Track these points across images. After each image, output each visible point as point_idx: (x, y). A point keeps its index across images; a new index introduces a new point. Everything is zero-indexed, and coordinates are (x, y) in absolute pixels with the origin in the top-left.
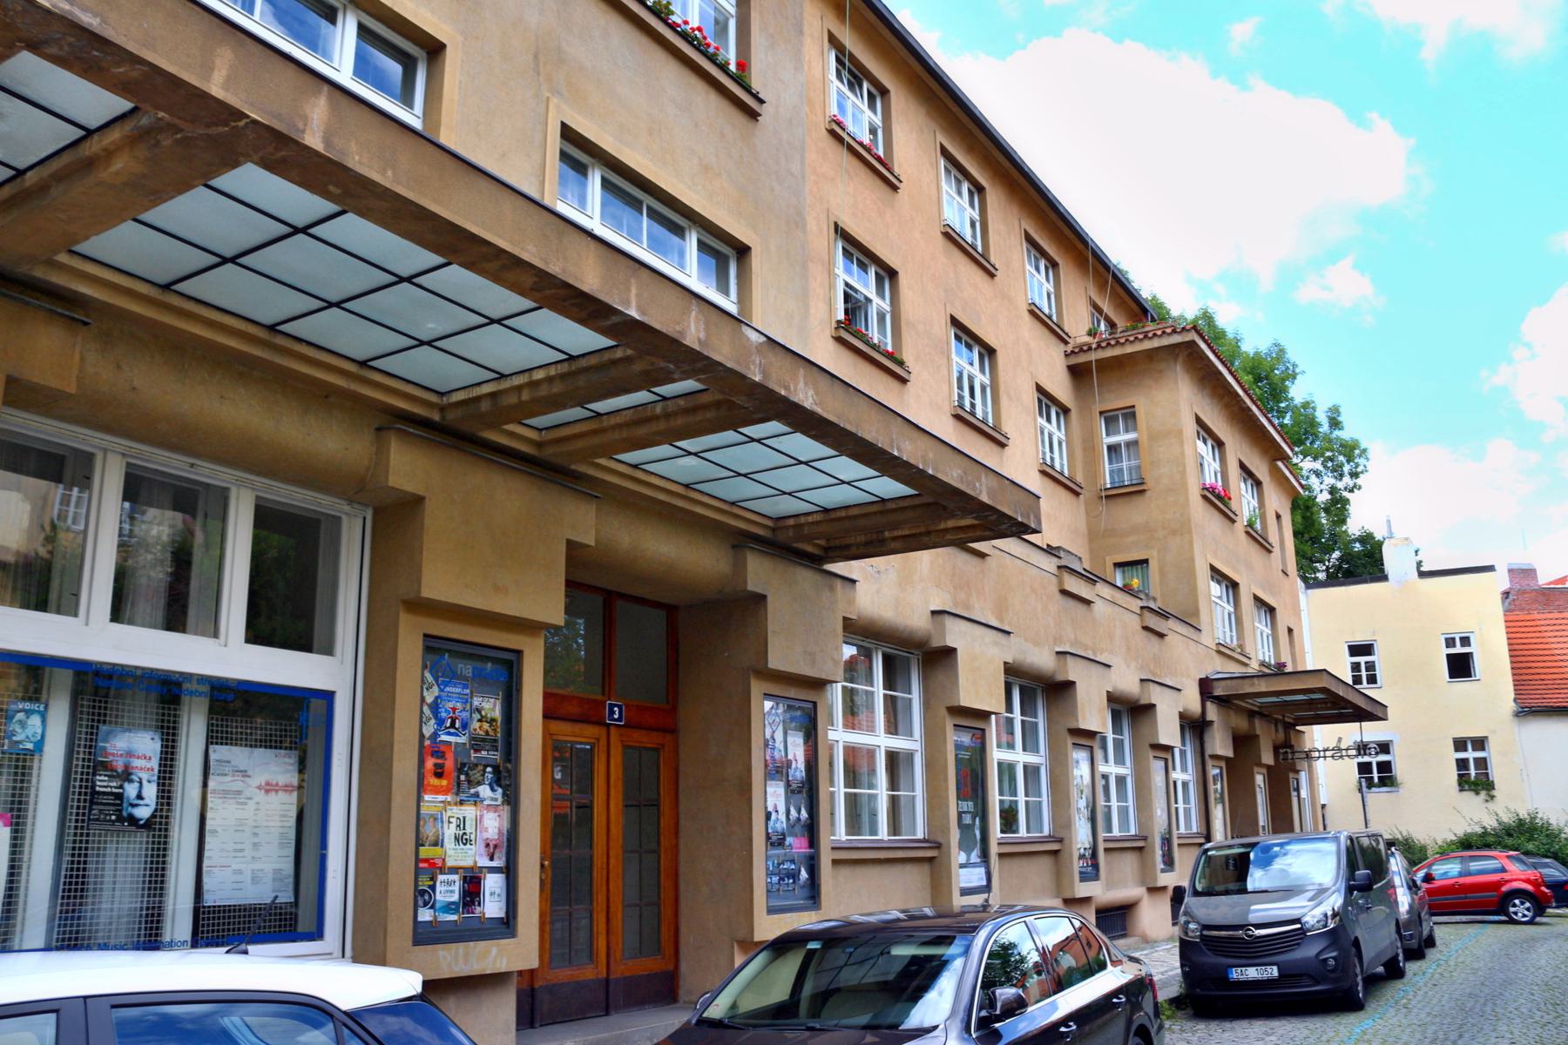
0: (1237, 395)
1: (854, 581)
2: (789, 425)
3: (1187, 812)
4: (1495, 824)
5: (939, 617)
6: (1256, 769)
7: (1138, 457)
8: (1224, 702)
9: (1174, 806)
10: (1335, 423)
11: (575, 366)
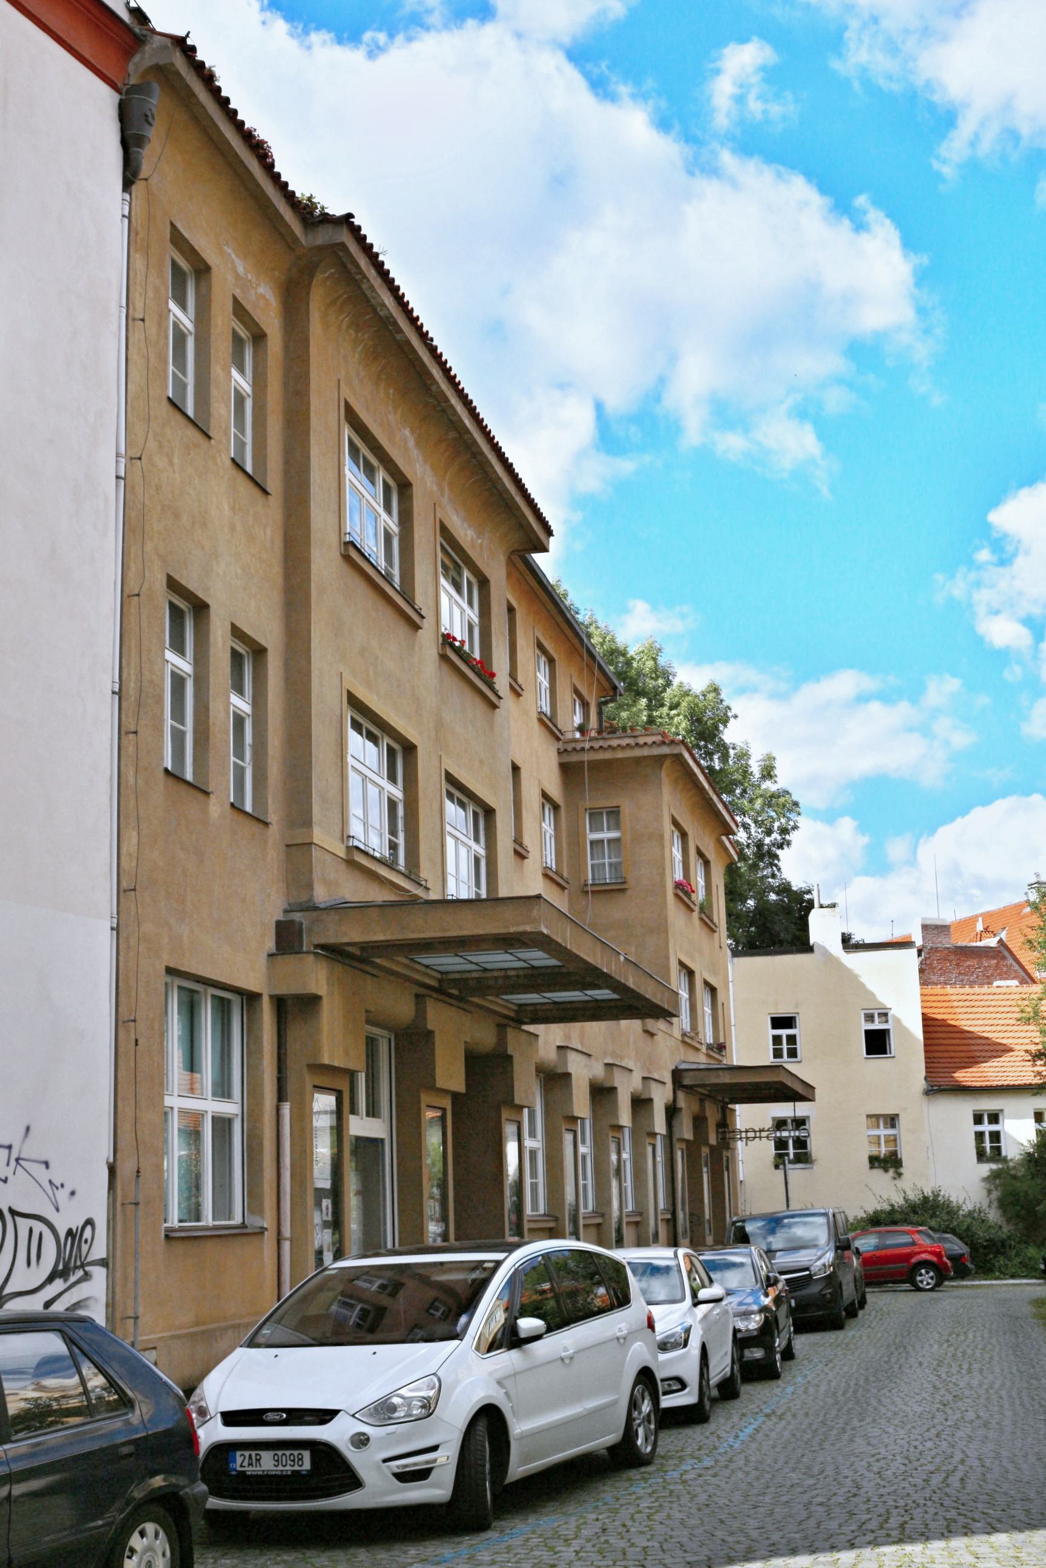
0: (704, 788)
1: (631, 1071)
2: (548, 953)
3: (534, 1187)
4: (902, 1202)
5: (563, 1051)
6: (425, 1098)
7: (618, 856)
8: (689, 1089)
9: (581, 1182)
10: (768, 773)
11: (535, 972)
